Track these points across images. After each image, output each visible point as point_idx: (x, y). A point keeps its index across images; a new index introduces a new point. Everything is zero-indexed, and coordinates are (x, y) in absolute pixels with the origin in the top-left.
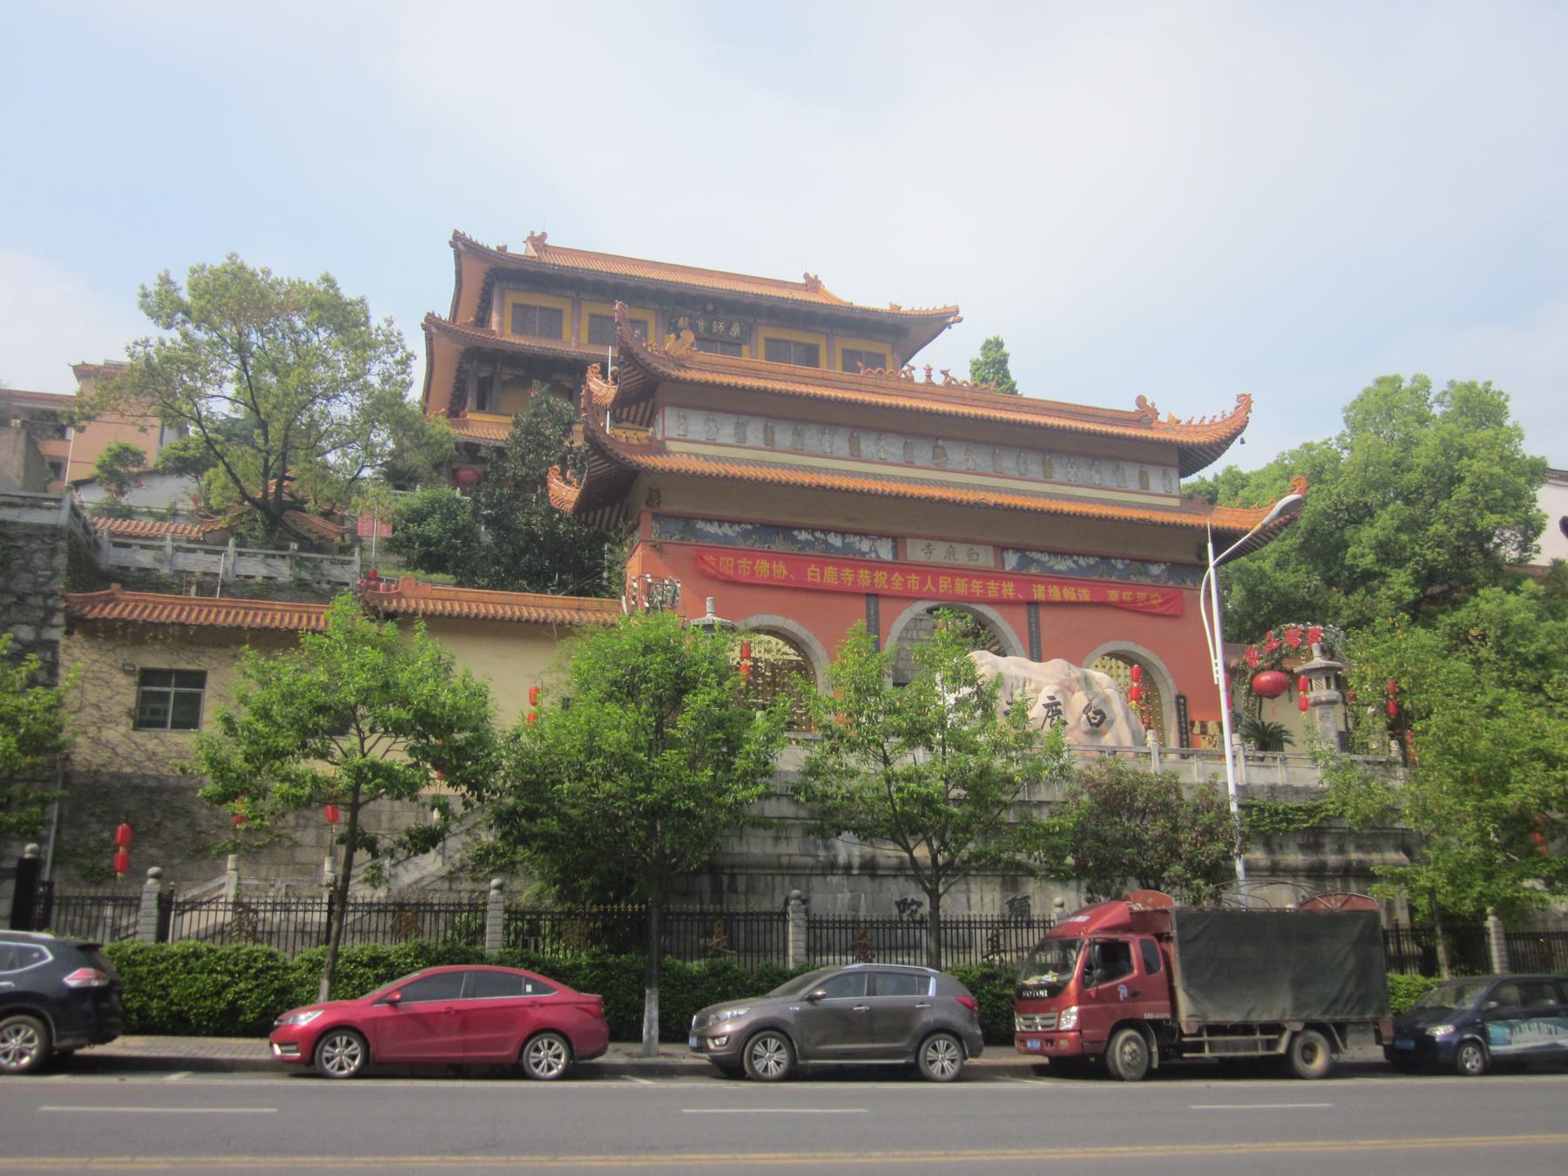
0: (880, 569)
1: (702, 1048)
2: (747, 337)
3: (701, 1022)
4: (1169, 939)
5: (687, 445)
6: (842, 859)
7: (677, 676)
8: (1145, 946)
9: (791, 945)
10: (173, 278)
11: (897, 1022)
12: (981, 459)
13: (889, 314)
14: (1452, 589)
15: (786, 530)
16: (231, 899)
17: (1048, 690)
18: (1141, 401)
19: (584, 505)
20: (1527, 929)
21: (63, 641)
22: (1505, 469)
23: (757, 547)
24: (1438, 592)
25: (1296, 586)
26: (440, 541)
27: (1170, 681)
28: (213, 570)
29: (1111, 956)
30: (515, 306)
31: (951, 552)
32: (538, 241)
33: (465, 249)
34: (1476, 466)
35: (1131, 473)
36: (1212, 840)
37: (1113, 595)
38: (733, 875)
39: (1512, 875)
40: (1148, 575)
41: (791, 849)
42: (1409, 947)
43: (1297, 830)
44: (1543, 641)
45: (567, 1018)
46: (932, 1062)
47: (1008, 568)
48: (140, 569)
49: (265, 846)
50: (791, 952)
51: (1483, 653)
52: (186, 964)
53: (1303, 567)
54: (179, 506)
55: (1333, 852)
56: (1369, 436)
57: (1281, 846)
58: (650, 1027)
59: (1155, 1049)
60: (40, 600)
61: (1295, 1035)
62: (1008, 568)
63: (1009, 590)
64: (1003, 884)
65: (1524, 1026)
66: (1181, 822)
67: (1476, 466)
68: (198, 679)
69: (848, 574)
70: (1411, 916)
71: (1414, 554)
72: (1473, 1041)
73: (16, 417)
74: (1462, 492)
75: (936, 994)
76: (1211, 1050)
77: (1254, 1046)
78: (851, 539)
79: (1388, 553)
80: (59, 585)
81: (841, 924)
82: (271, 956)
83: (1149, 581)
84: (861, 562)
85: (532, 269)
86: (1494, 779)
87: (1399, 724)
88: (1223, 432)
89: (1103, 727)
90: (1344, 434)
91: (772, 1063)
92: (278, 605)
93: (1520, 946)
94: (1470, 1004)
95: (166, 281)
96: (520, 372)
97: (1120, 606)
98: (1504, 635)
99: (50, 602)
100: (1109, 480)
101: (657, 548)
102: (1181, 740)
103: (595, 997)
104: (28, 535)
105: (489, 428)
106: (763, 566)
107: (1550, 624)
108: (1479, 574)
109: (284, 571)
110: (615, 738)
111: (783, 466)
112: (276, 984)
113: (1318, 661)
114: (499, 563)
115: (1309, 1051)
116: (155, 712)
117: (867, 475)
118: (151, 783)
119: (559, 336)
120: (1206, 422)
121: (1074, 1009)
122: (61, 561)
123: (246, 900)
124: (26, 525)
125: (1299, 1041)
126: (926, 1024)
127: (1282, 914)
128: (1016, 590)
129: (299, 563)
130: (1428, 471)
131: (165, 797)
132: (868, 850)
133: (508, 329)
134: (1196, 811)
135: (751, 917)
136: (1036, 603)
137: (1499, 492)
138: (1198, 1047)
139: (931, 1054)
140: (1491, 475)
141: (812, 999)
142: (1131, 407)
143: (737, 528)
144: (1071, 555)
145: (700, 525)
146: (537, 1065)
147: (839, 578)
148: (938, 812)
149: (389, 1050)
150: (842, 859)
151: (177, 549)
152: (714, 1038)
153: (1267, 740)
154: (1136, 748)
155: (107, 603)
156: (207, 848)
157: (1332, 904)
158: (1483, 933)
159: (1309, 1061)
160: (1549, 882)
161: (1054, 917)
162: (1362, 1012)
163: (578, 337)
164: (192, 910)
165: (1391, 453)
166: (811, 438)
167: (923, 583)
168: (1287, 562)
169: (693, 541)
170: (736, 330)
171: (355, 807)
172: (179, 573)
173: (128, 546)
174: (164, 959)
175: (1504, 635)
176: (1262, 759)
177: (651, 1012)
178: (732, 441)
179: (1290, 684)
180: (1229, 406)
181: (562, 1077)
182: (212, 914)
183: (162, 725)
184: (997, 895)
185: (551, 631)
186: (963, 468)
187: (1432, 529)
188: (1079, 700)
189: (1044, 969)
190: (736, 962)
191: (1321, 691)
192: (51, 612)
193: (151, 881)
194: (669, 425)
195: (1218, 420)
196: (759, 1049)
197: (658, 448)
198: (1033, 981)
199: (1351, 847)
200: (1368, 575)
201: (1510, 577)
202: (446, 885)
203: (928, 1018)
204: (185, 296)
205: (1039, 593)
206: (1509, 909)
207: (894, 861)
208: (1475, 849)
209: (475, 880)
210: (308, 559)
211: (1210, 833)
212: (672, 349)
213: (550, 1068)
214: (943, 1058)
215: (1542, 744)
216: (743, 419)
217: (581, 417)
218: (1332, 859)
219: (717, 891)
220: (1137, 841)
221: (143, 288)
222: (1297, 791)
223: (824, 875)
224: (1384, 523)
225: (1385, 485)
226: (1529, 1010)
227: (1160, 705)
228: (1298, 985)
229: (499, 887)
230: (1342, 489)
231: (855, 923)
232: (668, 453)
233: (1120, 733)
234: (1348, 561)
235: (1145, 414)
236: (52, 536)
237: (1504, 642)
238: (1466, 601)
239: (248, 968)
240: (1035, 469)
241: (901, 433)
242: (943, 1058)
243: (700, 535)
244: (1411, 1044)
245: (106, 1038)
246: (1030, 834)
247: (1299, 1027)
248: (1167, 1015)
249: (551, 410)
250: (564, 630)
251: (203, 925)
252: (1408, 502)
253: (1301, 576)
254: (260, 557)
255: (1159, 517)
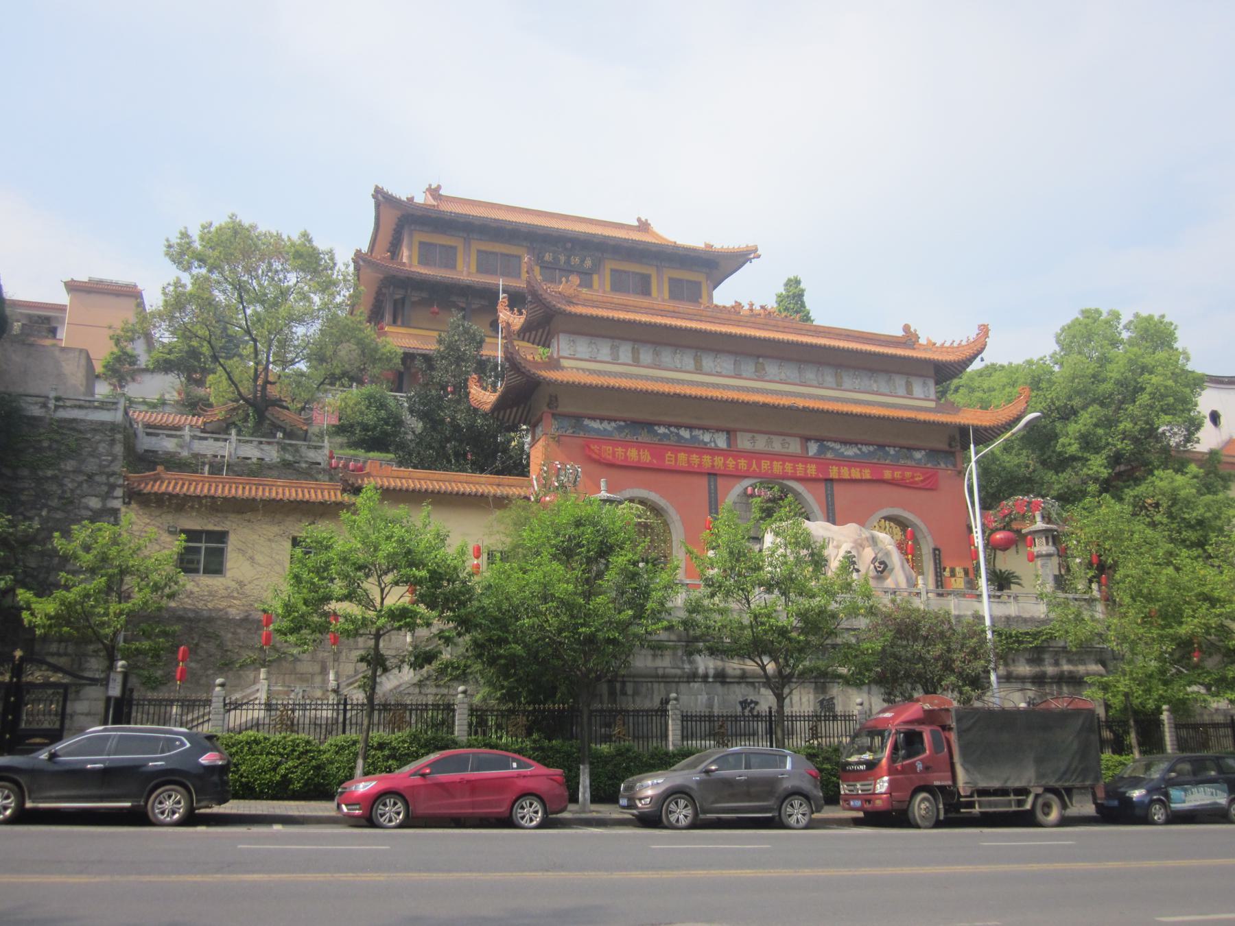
0: (718, 455)
1: (631, 806)
2: (596, 268)
3: (630, 788)
4: (950, 729)
5: (576, 363)
6: (701, 671)
7: (602, 542)
8: (933, 733)
9: (670, 733)
10: (190, 233)
11: (768, 787)
12: (790, 372)
13: (705, 252)
14: (1133, 469)
15: (649, 426)
16: (263, 701)
17: (846, 547)
18: (906, 328)
19: (500, 405)
20: (1192, 721)
21: (123, 509)
22: (1176, 382)
23: (629, 438)
24: (1127, 471)
25: (1019, 466)
26: (375, 428)
27: (929, 538)
28: (221, 453)
29: (911, 741)
30: (421, 243)
31: (770, 442)
32: (434, 192)
33: (383, 200)
34: (1155, 380)
35: (900, 382)
36: (975, 659)
37: (887, 475)
38: (624, 683)
39: (1183, 682)
40: (912, 458)
41: (665, 663)
42: (1107, 734)
43: (1026, 649)
44: (1202, 510)
45: (543, 786)
46: (790, 816)
47: (811, 454)
48: (167, 453)
49: (275, 660)
50: (670, 738)
51: (1158, 518)
52: (250, 748)
53: (1024, 452)
54: (167, 396)
55: (1050, 665)
56: (1075, 357)
57: (1014, 661)
58: (584, 793)
59: (941, 806)
60: (103, 479)
61: (1037, 796)
62: (811, 454)
63: (812, 470)
64: (816, 689)
65: (1194, 790)
66: (953, 646)
67: (1155, 380)
68: (222, 537)
69: (695, 458)
70: (1107, 711)
71: (1108, 444)
72: (1159, 800)
73: (18, 321)
74: (1144, 398)
75: (791, 768)
76: (980, 807)
77: (1009, 804)
78: (696, 432)
79: (1088, 443)
80: (118, 467)
81: (701, 718)
82: (308, 742)
83: (913, 463)
84: (705, 450)
85: (434, 215)
86: (1172, 615)
87: (1101, 569)
88: (968, 353)
89: (885, 573)
90: (1055, 353)
91: (681, 817)
92: (269, 481)
93: (1184, 733)
94: (1156, 774)
95: (184, 235)
96: (425, 295)
97: (892, 483)
98: (1173, 505)
99: (112, 480)
100: (884, 388)
101: (558, 440)
102: (937, 581)
103: (559, 771)
104: (94, 430)
105: (399, 340)
106: (633, 454)
107: (1209, 497)
108: (1153, 458)
109: (272, 454)
110: (563, 589)
111: (647, 378)
112: (314, 763)
113: (1040, 525)
114: (432, 448)
115: (1047, 807)
116: (191, 562)
117: (708, 385)
118: (191, 615)
119: (454, 267)
120: (955, 345)
121: (886, 778)
122: (119, 449)
123: (274, 702)
124: (91, 422)
125: (1040, 801)
126: (785, 789)
127: (1017, 712)
128: (818, 470)
129: (284, 448)
130: (1118, 383)
131: (201, 624)
132: (719, 663)
133: (415, 262)
134: (964, 638)
135: (637, 713)
136: (832, 480)
137: (1171, 400)
138: (971, 805)
139: (789, 810)
140: (1166, 387)
141: (707, 772)
142: (900, 333)
143: (613, 424)
144: (856, 444)
145: (586, 422)
146: (523, 818)
147: (688, 462)
148: (790, 639)
149: (422, 808)
150: (701, 671)
151: (194, 437)
152: (640, 799)
153: (1001, 581)
154: (908, 588)
155: (155, 481)
156: (232, 663)
157: (1059, 702)
158: (1159, 724)
159: (1047, 814)
160: (1208, 687)
161: (856, 712)
162: (1083, 781)
163: (469, 267)
164: (235, 709)
165: (1092, 368)
166: (667, 357)
167: (750, 465)
168: (1012, 448)
169: (582, 434)
170: (588, 263)
171: (378, 636)
172: (196, 456)
173: (157, 435)
174: (234, 745)
175: (1173, 505)
176: (999, 597)
177: (585, 781)
178: (608, 359)
179: (1018, 539)
180: (973, 334)
181: (539, 827)
182: (250, 712)
183: (196, 571)
184: (812, 696)
185: (488, 503)
186: (777, 379)
187: (1121, 426)
188: (869, 553)
189: (861, 751)
190: (638, 747)
191: (1042, 547)
192: (113, 487)
193: (218, 689)
194: (563, 346)
195: (964, 343)
196: (673, 806)
197: (554, 364)
198: (854, 759)
199: (1063, 662)
200: (1074, 458)
201: (1177, 460)
202: (417, 690)
203: (788, 784)
204: (197, 245)
205: (834, 473)
206: (1180, 707)
207: (738, 672)
208: (1153, 663)
209: (437, 686)
210: (291, 445)
211: (975, 653)
212: (567, 292)
213: (531, 820)
214: (797, 812)
215: (1206, 590)
216: (617, 342)
217: (479, 334)
218: (1050, 670)
219: (612, 693)
220: (921, 659)
221: (167, 240)
222: (1025, 621)
223: (688, 682)
224: (1083, 423)
225: (1086, 392)
226: (1197, 778)
227: (921, 555)
228: (1039, 761)
229: (464, 692)
230: (1058, 393)
231: (710, 718)
232: (563, 368)
233: (898, 577)
234: (1059, 448)
235: (909, 338)
236: (112, 430)
237: (1173, 510)
238: (1145, 479)
239: (294, 750)
240: (830, 379)
241: (729, 352)
242: (797, 812)
243: (587, 429)
244: (1116, 803)
245: (222, 800)
246: (848, 653)
247: (1040, 790)
248: (950, 783)
249: (466, 331)
250: (501, 502)
251: (244, 720)
252: (1102, 404)
253: (1023, 459)
254: (255, 443)
255: (922, 416)
